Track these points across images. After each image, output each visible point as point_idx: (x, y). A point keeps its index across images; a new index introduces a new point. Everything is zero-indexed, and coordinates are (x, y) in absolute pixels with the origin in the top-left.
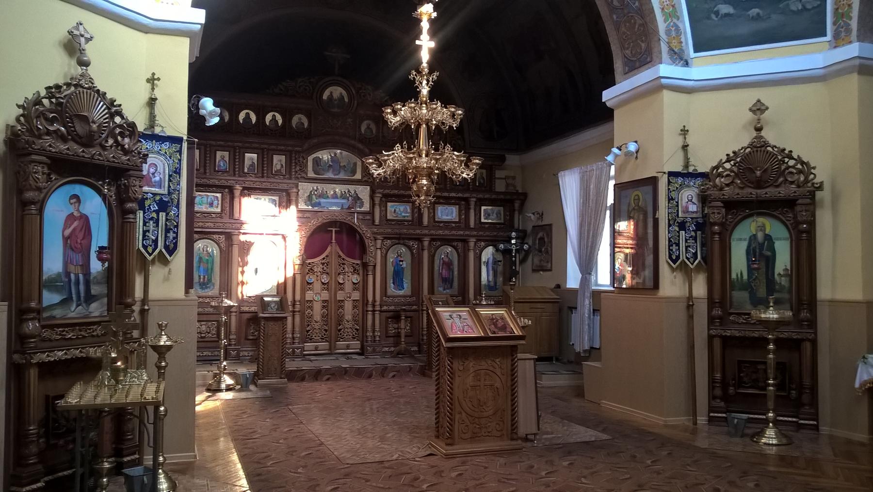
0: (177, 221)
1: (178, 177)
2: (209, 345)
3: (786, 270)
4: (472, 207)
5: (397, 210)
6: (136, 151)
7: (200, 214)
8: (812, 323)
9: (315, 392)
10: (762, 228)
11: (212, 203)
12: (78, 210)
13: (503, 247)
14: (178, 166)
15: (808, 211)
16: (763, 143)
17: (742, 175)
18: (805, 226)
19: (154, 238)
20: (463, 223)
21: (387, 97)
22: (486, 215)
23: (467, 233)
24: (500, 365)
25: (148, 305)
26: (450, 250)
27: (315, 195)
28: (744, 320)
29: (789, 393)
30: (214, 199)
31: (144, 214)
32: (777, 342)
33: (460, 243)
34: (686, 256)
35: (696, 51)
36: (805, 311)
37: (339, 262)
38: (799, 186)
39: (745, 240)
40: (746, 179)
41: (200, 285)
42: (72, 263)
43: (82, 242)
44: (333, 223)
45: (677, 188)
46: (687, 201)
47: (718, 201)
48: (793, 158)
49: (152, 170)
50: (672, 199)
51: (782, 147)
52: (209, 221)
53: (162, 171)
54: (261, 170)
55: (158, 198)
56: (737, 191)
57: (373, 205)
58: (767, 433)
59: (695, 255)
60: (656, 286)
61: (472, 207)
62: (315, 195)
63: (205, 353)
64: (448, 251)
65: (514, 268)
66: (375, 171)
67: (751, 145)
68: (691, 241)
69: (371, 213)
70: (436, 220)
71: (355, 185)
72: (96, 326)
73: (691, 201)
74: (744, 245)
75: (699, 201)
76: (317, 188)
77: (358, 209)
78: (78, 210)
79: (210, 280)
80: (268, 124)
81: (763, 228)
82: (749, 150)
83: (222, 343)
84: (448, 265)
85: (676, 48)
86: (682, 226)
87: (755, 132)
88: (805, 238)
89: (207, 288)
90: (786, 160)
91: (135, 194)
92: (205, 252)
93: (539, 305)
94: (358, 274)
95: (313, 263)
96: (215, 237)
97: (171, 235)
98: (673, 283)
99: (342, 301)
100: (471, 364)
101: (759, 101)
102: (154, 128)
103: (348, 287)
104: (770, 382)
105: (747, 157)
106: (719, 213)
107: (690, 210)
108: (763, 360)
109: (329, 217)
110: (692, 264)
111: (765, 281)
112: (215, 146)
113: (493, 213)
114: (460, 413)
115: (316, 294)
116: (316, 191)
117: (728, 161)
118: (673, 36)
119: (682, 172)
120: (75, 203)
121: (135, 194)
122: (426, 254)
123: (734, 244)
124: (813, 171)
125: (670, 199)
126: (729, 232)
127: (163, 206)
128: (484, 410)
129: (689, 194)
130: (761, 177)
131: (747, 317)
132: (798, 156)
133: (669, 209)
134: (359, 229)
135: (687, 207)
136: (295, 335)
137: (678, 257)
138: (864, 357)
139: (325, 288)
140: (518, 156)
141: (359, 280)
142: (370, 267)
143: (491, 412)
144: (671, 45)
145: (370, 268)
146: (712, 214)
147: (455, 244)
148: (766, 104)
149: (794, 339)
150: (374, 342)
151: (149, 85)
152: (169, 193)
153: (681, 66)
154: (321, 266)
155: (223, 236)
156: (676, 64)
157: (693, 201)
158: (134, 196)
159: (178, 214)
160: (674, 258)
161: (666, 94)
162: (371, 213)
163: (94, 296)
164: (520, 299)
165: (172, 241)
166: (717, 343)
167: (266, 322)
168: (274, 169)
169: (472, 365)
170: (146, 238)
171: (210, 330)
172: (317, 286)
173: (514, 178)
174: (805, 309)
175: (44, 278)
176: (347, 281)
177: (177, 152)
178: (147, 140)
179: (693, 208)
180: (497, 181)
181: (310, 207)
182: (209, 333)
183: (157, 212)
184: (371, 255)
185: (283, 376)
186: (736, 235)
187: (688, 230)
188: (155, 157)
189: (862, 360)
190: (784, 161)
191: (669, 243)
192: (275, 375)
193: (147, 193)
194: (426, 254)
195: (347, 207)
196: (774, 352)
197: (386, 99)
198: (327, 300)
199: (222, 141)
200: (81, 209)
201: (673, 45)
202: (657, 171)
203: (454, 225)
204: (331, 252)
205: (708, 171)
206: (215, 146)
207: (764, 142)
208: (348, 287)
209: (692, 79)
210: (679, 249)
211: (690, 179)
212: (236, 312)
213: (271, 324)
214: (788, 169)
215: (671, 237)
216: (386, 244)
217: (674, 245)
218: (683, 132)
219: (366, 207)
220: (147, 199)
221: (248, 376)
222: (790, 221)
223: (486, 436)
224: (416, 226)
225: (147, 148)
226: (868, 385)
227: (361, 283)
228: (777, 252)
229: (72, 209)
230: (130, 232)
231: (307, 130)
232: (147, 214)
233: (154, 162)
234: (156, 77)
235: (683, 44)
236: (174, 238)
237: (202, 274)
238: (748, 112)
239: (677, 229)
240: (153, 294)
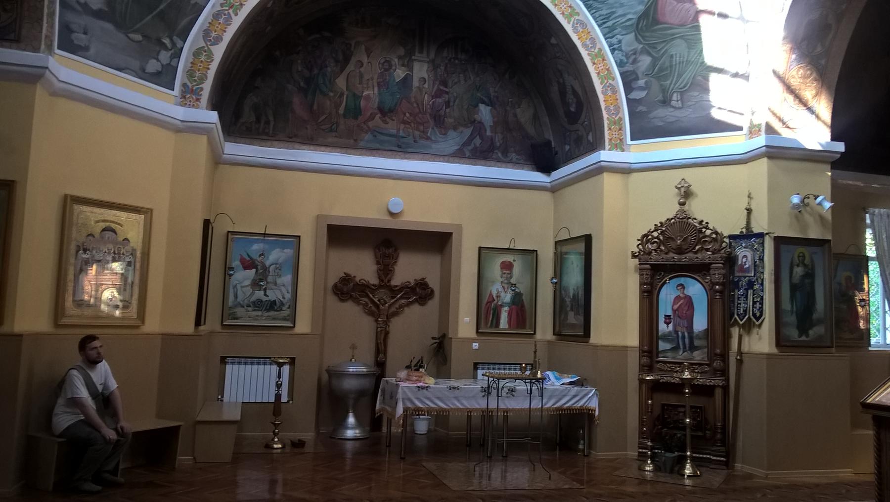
12: (683, 293)
19: (745, 309)
28: (669, 368)
35: (632, 140)
38: (714, 253)
42: (679, 325)
43: (688, 312)
49: (744, 260)
56: (664, 256)
67: (675, 217)
68: (742, 299)
78: (683, 293)
82: (673, 220)
87: (679, 206)
90: (704, 230)
97: (758, 305)
117: (656, 230)
120: (681, 289)
131: (671, 365)
132: (714, 227)
163: (697, 347)
175: (660, 334)
183: (747, 290)
190: (702, 231)
200: (685, 292)
228: (695, 309)
229: (678, 293)
236: (760, 308)
238: (675, 188)
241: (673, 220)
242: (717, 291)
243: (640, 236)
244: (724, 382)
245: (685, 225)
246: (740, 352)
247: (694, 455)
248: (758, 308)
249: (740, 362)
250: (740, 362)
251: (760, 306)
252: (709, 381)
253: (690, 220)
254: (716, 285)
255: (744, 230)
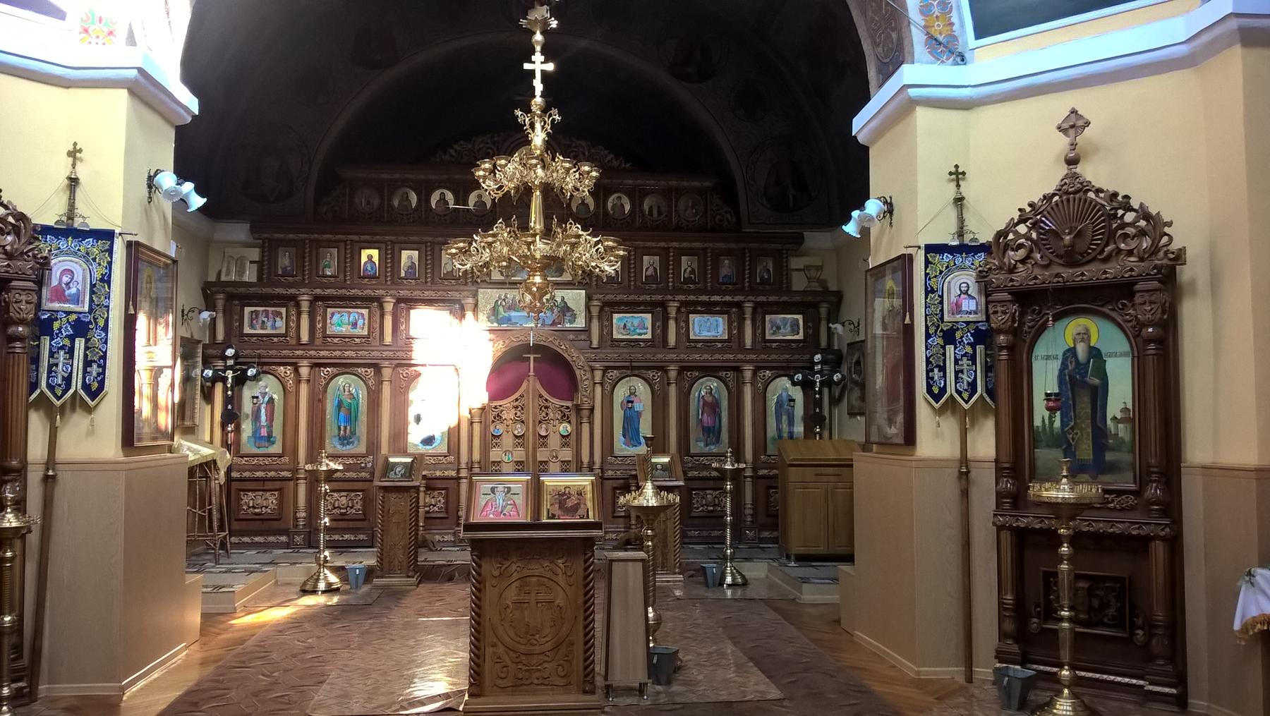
0: (104, 350)
1: (106, 286)
2: (351, 524)
3: (1125, 410)
4: (748, 315)
5: (629, 325)
6: (30, 254)
7: (338, 339)
8: (1171, 508)
9: (665, 596)
10: (1085, 336)
11: (356, 324)
13: (800, 378)
14: (108, 271)
15: (1155, 303)
16: (1079, 185)
17: (1045, 245)
18: (1150, 330)
19: (66, 375)
20: (734, 341)
21: (612, 156)
22: (774, 329)
23: (740, 356)
24: (561, 571)
25: (54, 470)
26: (715, 384)
27: (503, 306)
29: (1132, 634)
30: (359, 317)
31: (51, 341)
32: (1076, 540)
33: (728, 371)
34: (956, 387)
36: (1154, 485)
37: (540, 405)
38: (1142, 260)
39: (1056, 358)
40: (1051, 251)
41: (340, 439)
44: (526, 348)
45: (941, 272)
46: (959, 293)
47: (1002, 291)
48: (1130, 209)
49: (65, 279)
50: (933, 291)
51: (1112, 189)
52: (362, 348)
53: (80, 279)
54: (627, 272)
55: (74, 317)
57: (589, 319)
58: (1058, 707)
59: (973, 386)
60: (910, 438)
61: (748, 315)
62: (503, 306)
63: (346, 537)
64: (712, 387)
65: (818, 410)
66: (460, 267)
67: (1059, 190)
68: (965, 361)
69: (587, 330)
70: (767, 338)
71: (485, 288)
72: (1112, 496)
73: (966, 293)
74: (1055, 366)
75: (980, 292)
76: (506, 296)
77: (568, 325)
79: (353, 433)
80: (434, 207)
81: (1085, 336)
83: (320, 523)
84: (712, 407)
85: (940, 34)
86: (949, 337)
88: (1153, 352)
89: (348, 444)
91: (20, 314)
92: (346, 393)
93: (831, 470)
94: (569, 422)
95: (500, 406)
96: (359, 371)
97: (95, 369)
98: (937, 435)
99: (546, 462)
100: (514, 567)
101: (1074, 112)
102: (73, 220)
103: (554, 442)
104: (1063, 613)
105: (1055, 208)
106: (1004, 313)
107: (963, 309)
108: (1051, 570)
109: (521, 338)
110: (967, 402)
111: (1090, 430)
112: (357, 242)
113: (786, 324)
114: (494, 645)
115: (506, 452)
116: (504, 300)
117: (1022, 220)
118: (935, 16)
119: (969, 244)
121: (20, 314)
122: (673, 390)
123: (1038, 366)
124: (1166, 230)
125: (929, 291)
126: (1027, 345)
127: (81, 328)
128: (536, 643)
129: (962, 281)
130: (1072, 245)
132: (1141, 204)
133: (926, 308)
134: (566, 355)
135: (958, 305)
136: (298, 515)
137: (943, 390)
138: (1249, 574)
139: (519, 444)
140: (829, 233)
141: (570, 431)
142: (584, 411)
143: (549, 646)
144: (932, 31)
145: (585, 413)
146: (993, 314)
147: (650, 374)
148: (1087, 116)
149: (1134, 535)
150: (296, 528)
151: (70, 160)
152: (91, 310)
153: (952, 65)
154: (513, 410)
155: (372, 369)
156: (943, 62)
157: (969, 293)
158: (18, 316)
159: (107, 339)
160: (936, 390)
161: (922, 114)
162: (587, 330)
164: (797, 460)
165: (96, 378)
166: (1006, 536)
167: (386, 494)
168: (444, 271)
169: (515, 567)
170: (53, 374)
171: (353, 503)
172: (508, 441)
173: (820, 268)
174: (1155, 481)
176: (552, 433)
177: (106, 251)
178: (60, 237)
179: (968, 305)
180: (795, 274)
181: (495, 325)
182: (351, 508)
183: (72, 338)
184: (585, 393)
185: (410, 574)
186: (1040, 349)
187: (960, 342)
188: (71, 261)
189: (1247, 578)
191: (927, 366)
192: (399, 572)
193: (58, 311)
194: (673, 390)
195: (550, 323)
196: (1071, 560)
197: (608, 158)
198: (523, 462)
199: (368, 235)
201: (936, 30)
202: (906, 245)
203: (719, 345)
204: (527, 391)
205: (991, 240)
206: (357, 242)
207: (1081, 183)
208: (554, 442)
209: (967, 84)
210: (945, 376)
211: (964, 255)
212: (751, 477)
213: (393, 497)
214: (1123, 229)
215: (930, 357)
216: (611, 376)
217: (936, 370)
218: (954, 177)
219: (580, 323)
220: (958, 329)
221: (715, 571)
222: (1130, 321)
223: (538, 685)
224: (659, 348)
225: (59, 248)
226: (1259, 626)
227: (573, 437)
230: (13, 368)
231: (491, 211)
232: (55, 340)
233: (70, 268)
234: (78, 148)
235: (955, 28)
236: (99, 374)
237: (342, 424)
239: (941, 341)
240: (64, 453)
241: (1056, 198)
242: (1149, 340)
243: (992, 236)
244: (1167, 530)
245: (1062, 210)
246: (51, 462)
247: (1055, 670)
248: (94, 374)
249: (49, 481)
250: (49, 481)
251: (100, 370)
252: (1137, 526)
253: (1091, 195)
254: (1148, 326)
255: (64, 219)
